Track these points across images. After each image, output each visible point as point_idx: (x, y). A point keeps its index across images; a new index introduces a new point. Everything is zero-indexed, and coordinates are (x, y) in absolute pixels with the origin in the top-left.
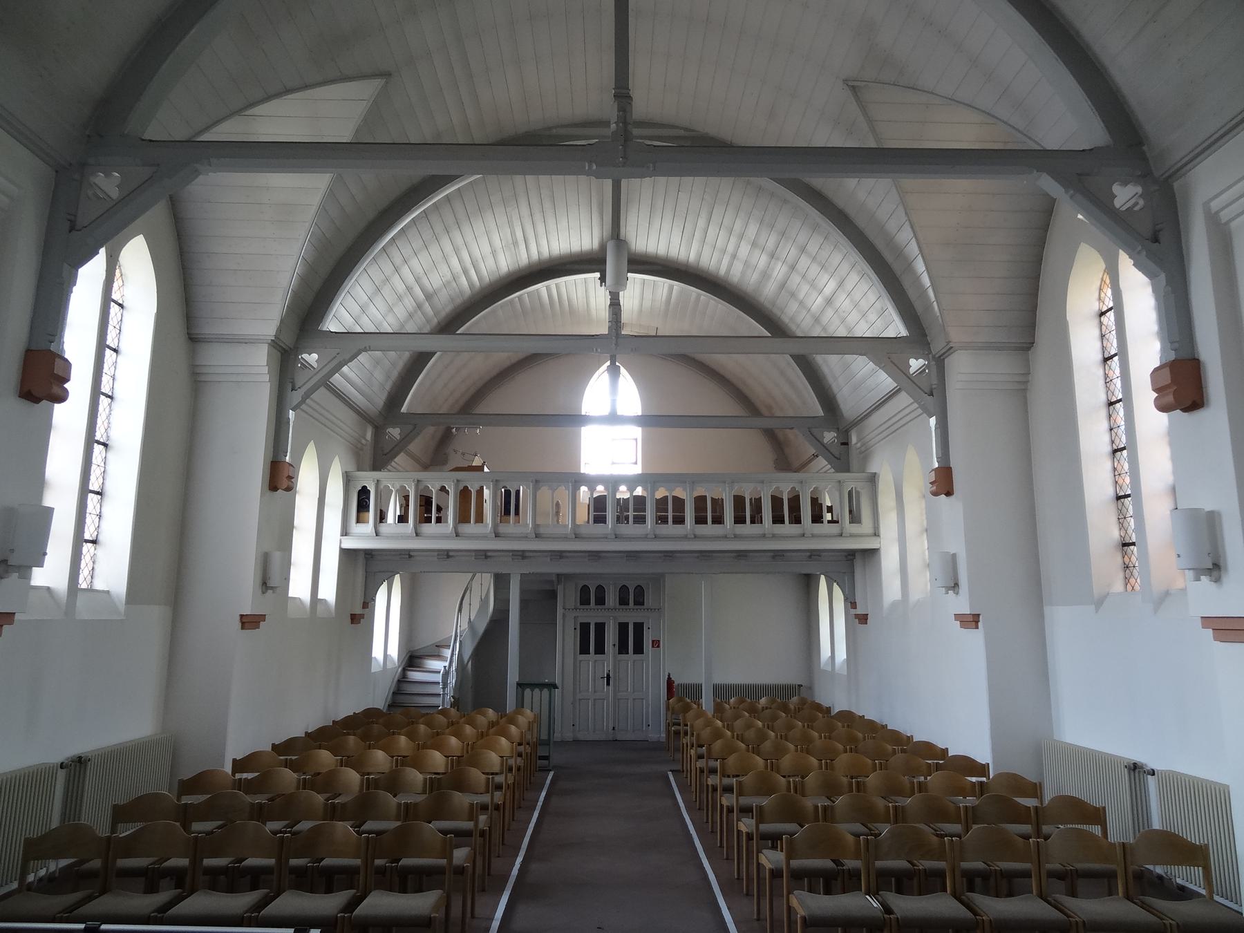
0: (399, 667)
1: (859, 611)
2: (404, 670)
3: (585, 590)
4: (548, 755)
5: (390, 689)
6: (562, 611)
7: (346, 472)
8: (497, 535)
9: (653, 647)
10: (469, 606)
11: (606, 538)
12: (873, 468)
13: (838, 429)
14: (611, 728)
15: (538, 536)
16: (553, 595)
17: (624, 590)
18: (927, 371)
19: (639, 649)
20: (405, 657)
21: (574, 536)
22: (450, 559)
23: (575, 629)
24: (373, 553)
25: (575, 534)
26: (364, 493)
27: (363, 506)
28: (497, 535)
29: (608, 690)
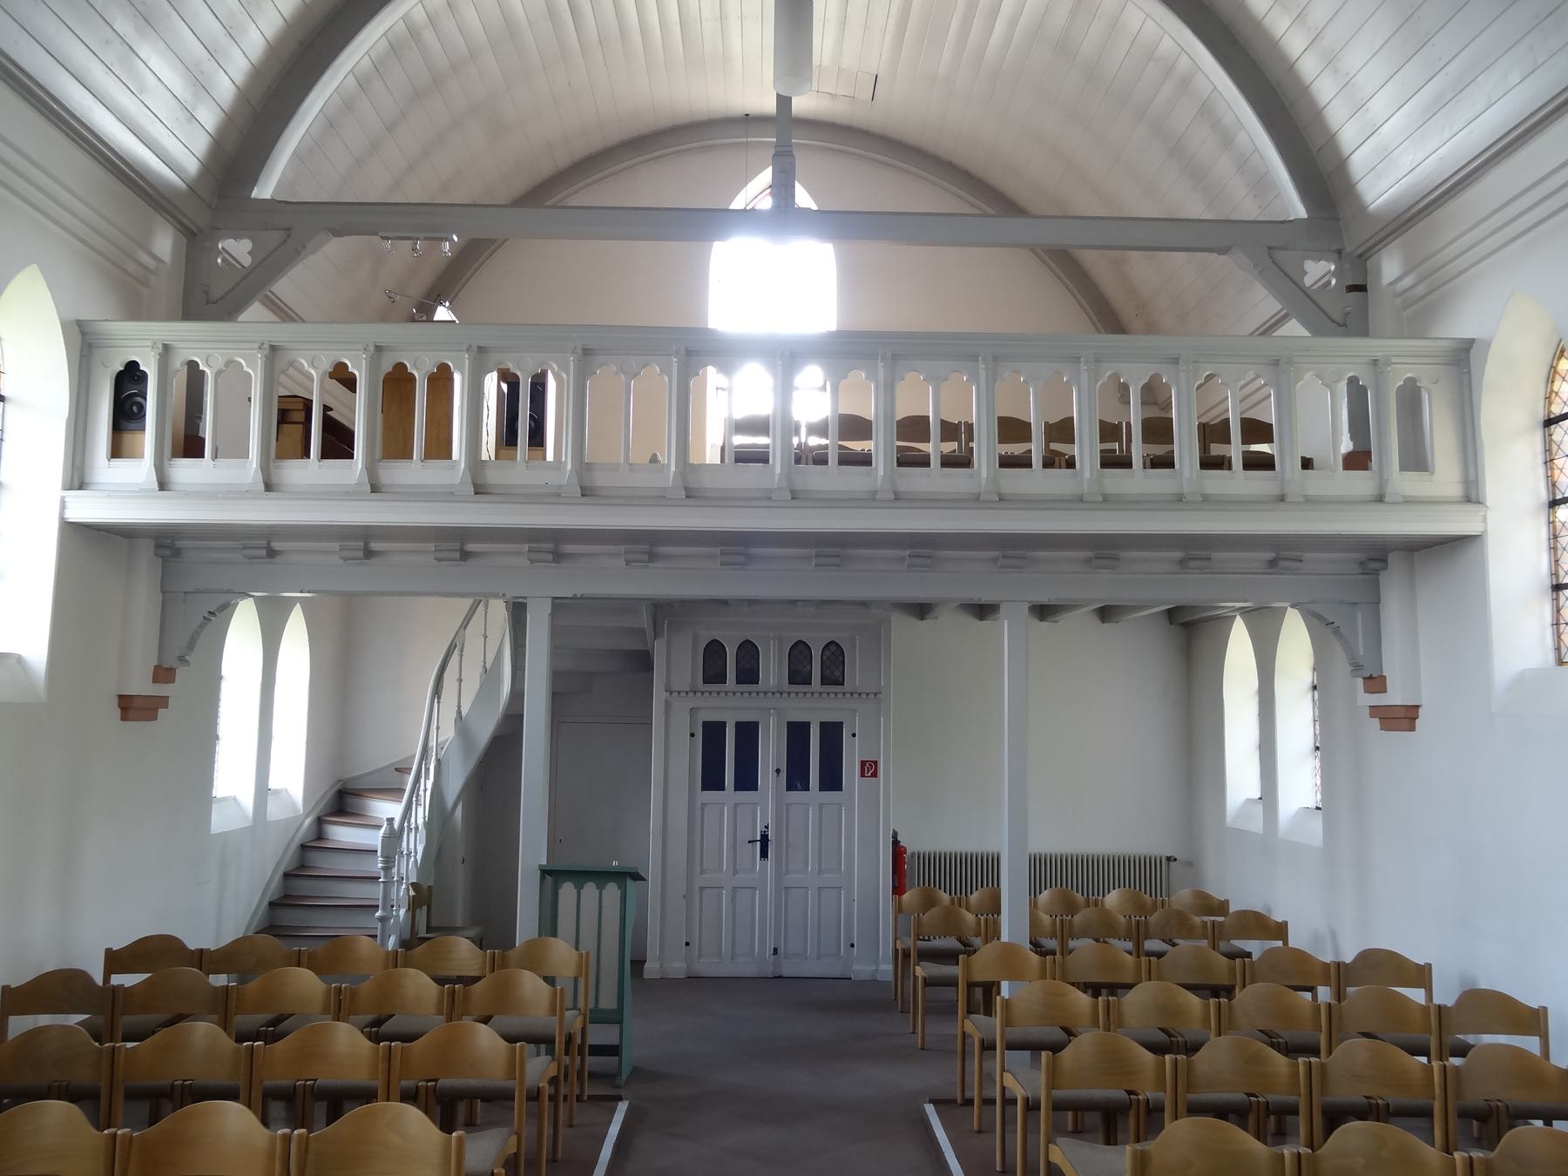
0: (307, 816)
1: (1395, 696)
2: (320, 822)
3: (714, 650)
4: (616, 1042)
5: (278, 864)
6: (665, 695)
7: (79, 323)
8: (480, 490)
9: (863, 775)
10: (457, 683)
11: (770, 498)
12: (1463, 324)
13: (1339, 252)
14: (769, 951)
15: (586, 492)
16: (642, 662)
17: (799, 653)
18: (1334, 282)
19: (831, 780)
20: (320, 800)
21: (683, 494)
22: (374, 561)
23: (692, 735)
24: (179, 544)
25: (686, 489)
26: (130, 377)
27: (126, 414)
28: (480, 490)
29: (764, 869)
